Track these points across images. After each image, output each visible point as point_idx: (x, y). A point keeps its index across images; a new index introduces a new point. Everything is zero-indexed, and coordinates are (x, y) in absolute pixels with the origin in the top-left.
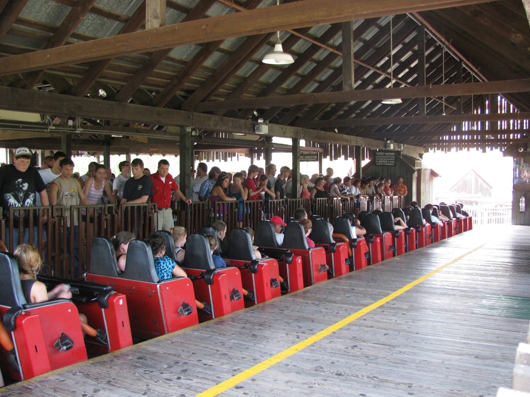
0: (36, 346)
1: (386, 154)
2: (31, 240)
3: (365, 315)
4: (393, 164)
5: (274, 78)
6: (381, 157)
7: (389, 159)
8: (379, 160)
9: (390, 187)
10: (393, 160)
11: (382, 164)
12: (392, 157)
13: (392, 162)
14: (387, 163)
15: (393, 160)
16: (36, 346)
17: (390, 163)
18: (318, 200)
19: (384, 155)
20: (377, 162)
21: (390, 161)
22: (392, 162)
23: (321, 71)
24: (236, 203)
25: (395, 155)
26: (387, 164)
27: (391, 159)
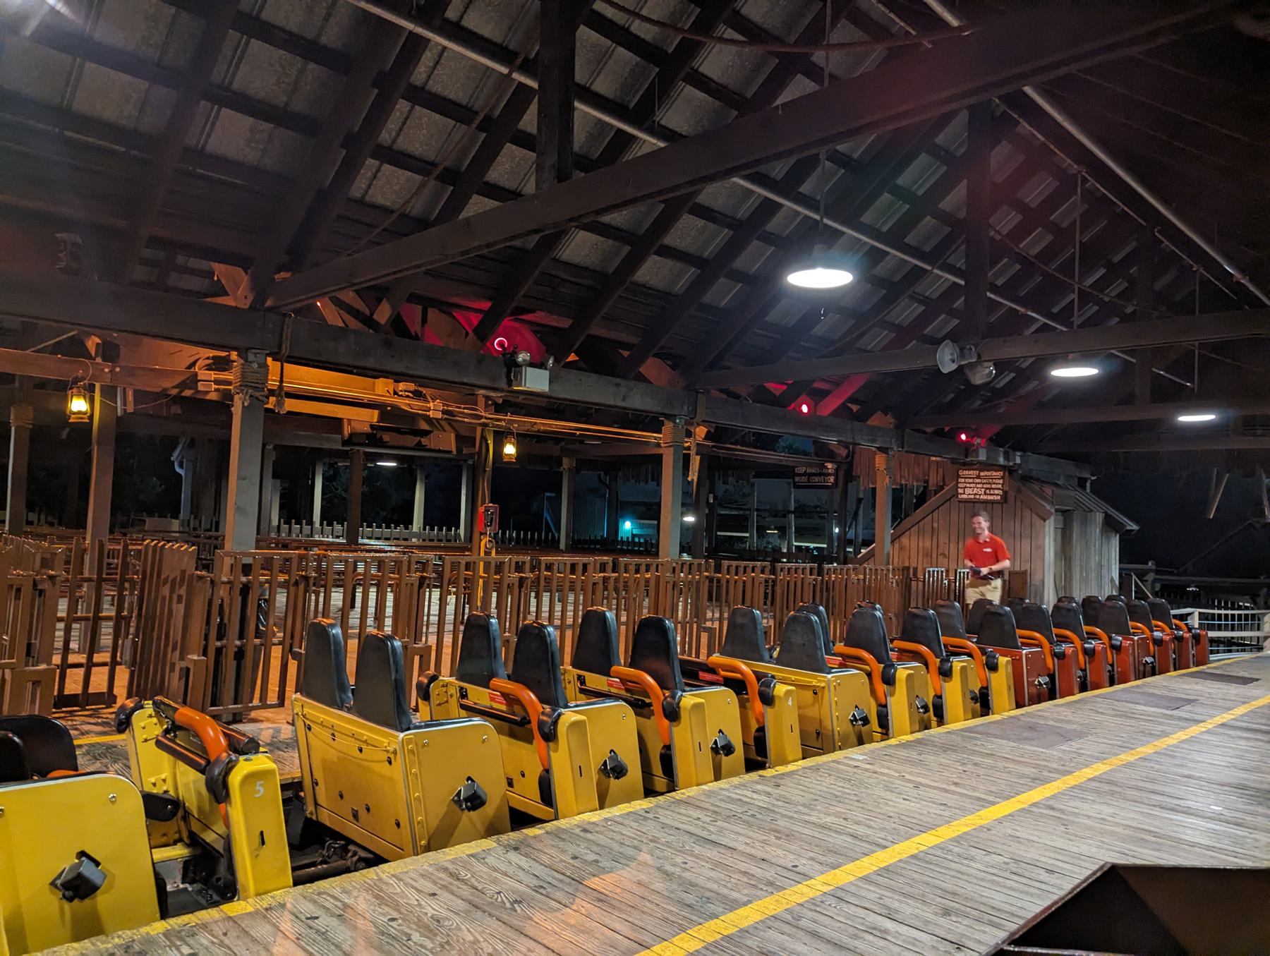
0: (262, 833)
1: (982, 474)
2: (812, 588)
3: (1054, 797)
4: (999, 498)
5: (616, 262)
6: (971, 481)
7: (988, 486)
8: (966, 487)
9: (1177, 568)
10: (999, 489)
11: (972, 496)
12: (997, 481)
13: (996, 492)
14: (985, 494)
15: (999, 489)
16: (262, 833)
17: (991, 495)
18: (929, 572)
19: (978, 477)
20: (960, 491)
21: (990, 489)
22: (996, 492)
23: (384, 9)
24: (398, 563)
25: (1003, 478)
26: (985, 497)
27: (993, 486)
